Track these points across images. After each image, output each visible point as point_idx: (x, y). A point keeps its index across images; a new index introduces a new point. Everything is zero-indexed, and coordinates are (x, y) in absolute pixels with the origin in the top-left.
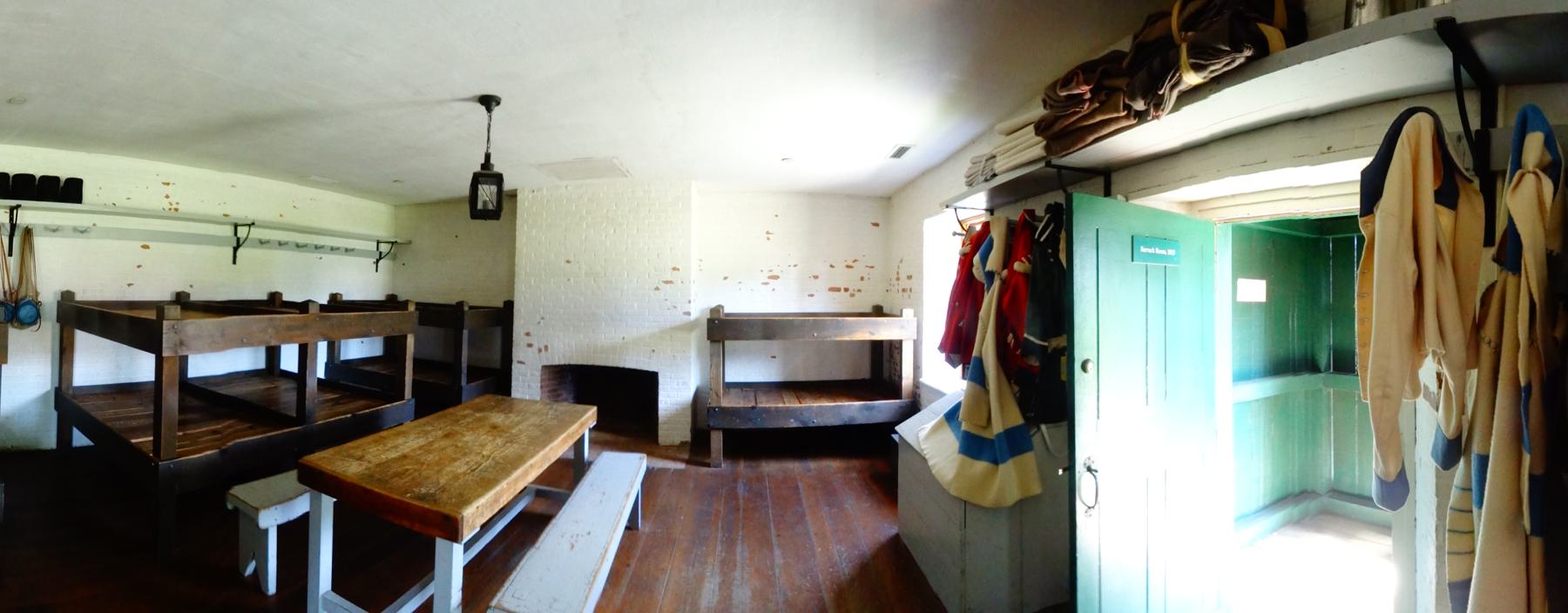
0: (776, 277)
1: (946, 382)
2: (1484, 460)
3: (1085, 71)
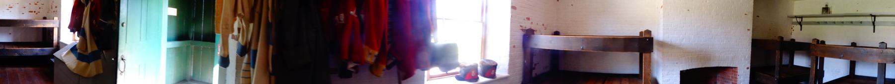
2: (255, 52)
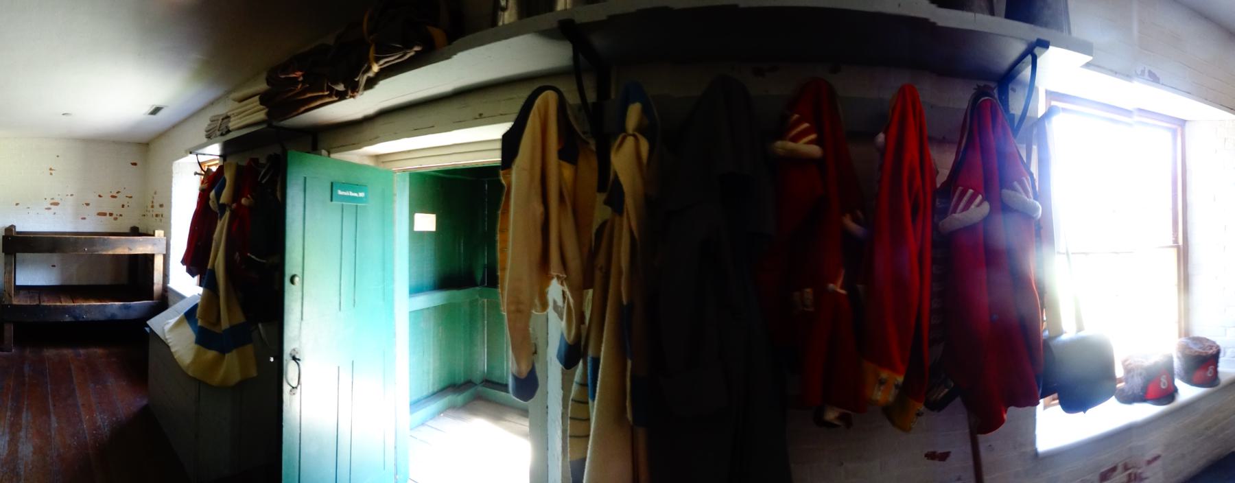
0: (56, 204)
1: (187, 286)
2: (596, 361)
3: (296, 61)
